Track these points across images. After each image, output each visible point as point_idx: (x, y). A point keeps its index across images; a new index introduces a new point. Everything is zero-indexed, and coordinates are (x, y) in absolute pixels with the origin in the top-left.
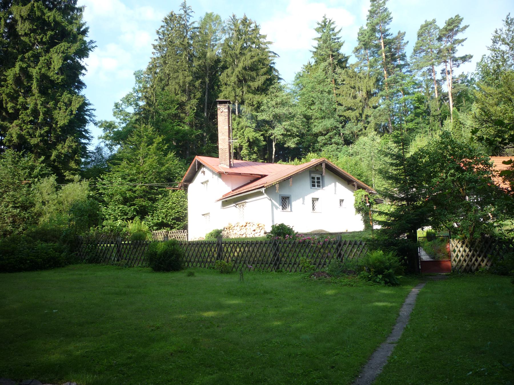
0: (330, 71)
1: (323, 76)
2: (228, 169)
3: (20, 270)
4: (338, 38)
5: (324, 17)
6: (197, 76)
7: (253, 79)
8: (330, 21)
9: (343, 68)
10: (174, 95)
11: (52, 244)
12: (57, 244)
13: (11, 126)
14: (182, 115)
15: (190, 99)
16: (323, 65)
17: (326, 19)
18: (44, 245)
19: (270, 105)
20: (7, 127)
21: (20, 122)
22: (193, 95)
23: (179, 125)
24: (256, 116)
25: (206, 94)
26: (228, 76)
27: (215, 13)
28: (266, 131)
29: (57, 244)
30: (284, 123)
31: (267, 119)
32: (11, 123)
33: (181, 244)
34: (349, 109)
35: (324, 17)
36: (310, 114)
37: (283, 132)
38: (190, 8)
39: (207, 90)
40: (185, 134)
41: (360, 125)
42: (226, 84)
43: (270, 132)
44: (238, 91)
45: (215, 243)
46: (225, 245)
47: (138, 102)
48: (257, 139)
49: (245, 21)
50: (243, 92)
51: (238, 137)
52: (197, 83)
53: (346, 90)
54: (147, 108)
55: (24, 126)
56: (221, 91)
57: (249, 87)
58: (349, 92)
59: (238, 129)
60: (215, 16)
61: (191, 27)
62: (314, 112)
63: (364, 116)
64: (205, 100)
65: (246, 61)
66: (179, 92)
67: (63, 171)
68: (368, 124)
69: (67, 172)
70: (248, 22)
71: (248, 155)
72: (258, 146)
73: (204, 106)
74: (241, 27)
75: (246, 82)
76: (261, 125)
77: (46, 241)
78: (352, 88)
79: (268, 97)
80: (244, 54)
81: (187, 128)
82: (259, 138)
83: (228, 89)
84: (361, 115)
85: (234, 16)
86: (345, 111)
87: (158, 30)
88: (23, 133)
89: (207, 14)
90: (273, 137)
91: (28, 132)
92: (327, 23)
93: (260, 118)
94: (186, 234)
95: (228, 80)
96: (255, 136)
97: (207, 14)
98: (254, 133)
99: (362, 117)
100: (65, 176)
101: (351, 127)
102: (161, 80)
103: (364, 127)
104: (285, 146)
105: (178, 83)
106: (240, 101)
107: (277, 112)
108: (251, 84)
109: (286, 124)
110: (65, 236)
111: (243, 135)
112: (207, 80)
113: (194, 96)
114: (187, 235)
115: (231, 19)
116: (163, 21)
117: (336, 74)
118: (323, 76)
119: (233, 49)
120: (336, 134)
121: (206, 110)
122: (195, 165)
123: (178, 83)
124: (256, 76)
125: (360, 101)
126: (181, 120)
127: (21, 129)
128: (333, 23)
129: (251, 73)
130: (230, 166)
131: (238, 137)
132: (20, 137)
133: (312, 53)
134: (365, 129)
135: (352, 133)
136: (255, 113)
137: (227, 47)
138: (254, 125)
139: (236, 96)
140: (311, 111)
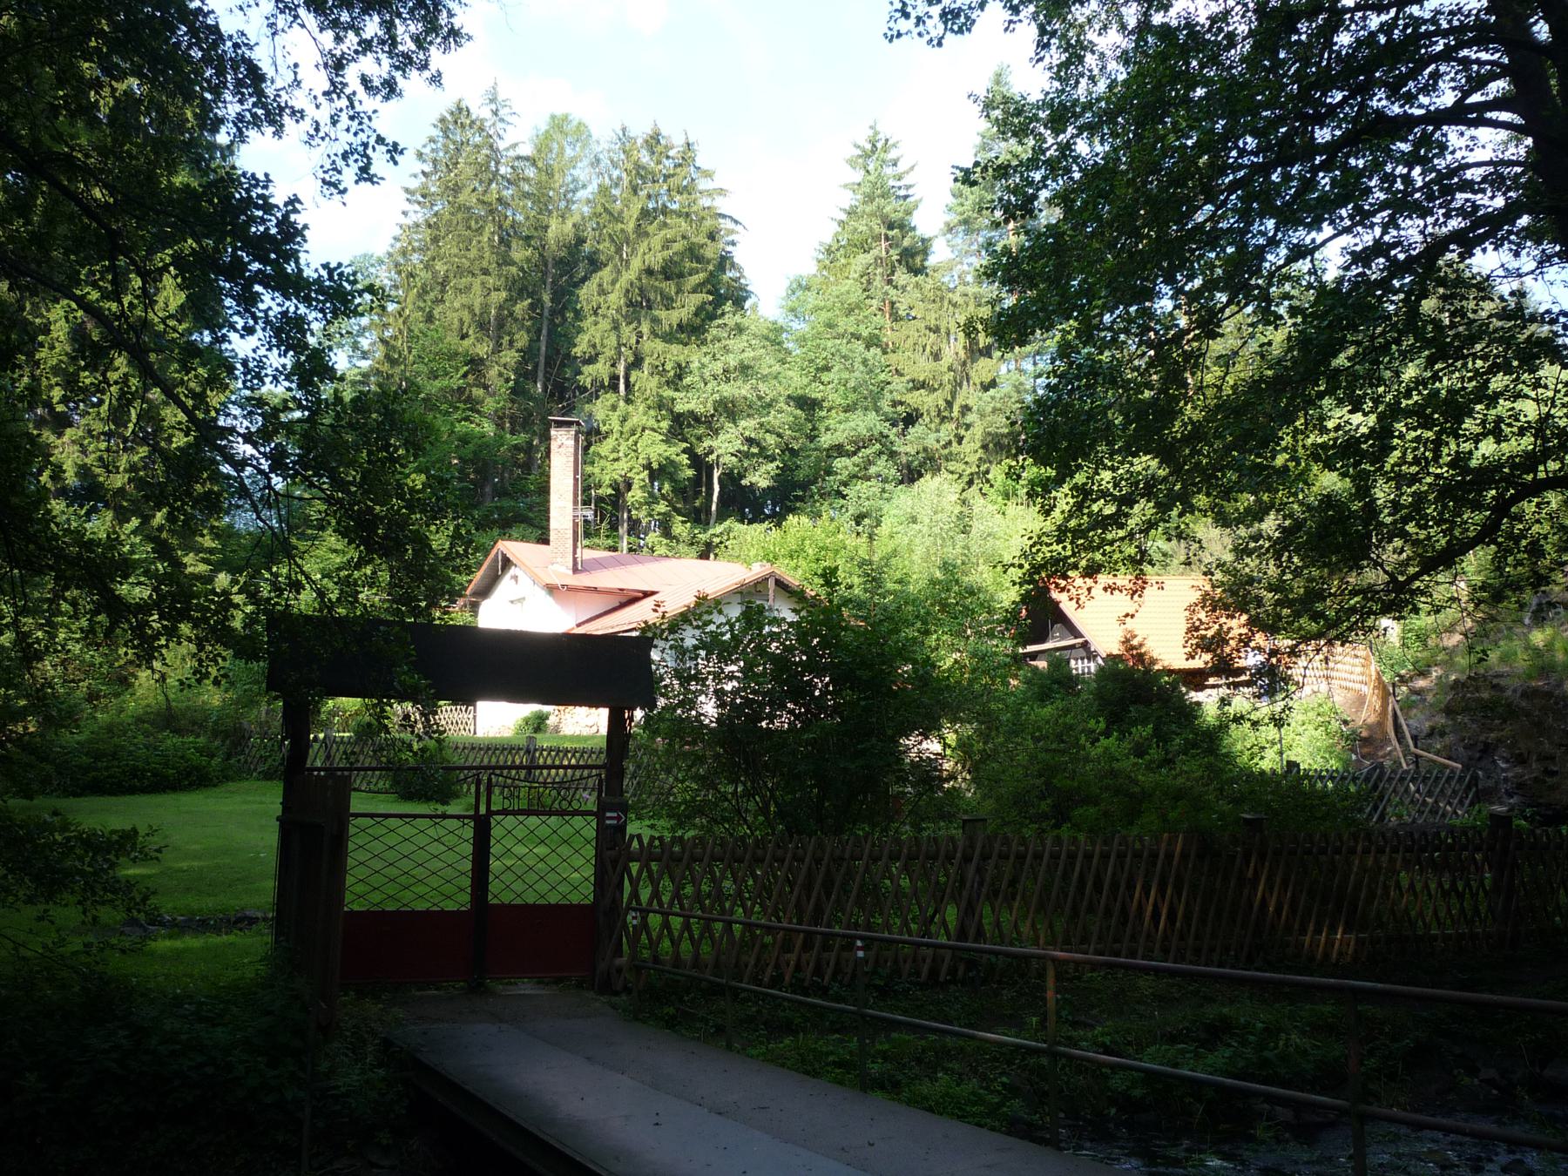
0: (878, 282)
1: (856, 295)
2: (567, 575)
3: (132, 791)
4: (908, 187)
5: (871, 127)
6: (519, 288)
7: (668, 303)
8: (887, 140)
9: (917, 271)
10: (457, 340)
11: (191, 739)
12: (202, 740)
13: (59, 441)
14: (478, 392)
15: (498, 348)
16: (863, 259)
17: (876, 133)
18: (177, 740)
19: (707, 374)
20: (49, 445)
21: (80, 433)
22: (508, 338)
23: (466, 419)
24: (673, 400)
25: (544, 332)
26: (602, 292)
27: (576, 116)
28: (699, 439)
29: (202, 740)
30: (743, 423)
31: (700, 409)
32: (60, 435)
33: (457, 748)
34: (918, 385)
35: (871, 127)
36: (819, 396)
37: (738, 445)
38: (508, 103)
39: (545, 323)
40: (483, 445)
41: (948, 430)
42: (595, 313)
43: (707, 443)
44: (627, 331)
45: (520, 749)
46: (541, 754)
47: (359, 339)
48: (672, 462)
49: (654, 141)
50: (640, 335)
51: (621, 454)
52: (521, 307)
53: (916, 334)
54: (386, 368)
55: (90, 443)
56: (580, 330)
57: (656, 321)
58: (922, 341)
59: (622, 433)
60: (575, 123)
61: (512, 153)
62: (829, 392)
63: (956, 408)
64: (539, 350)
65: (651, 253)
66: (471, 332)
67: (179, 553)
68: (967, 430)
69: (191, 555)
70: (663, 142)
71: (647, 503)
72: (672, 480)
73: (536, 366)
74: (645, 158)
75: (650, 308)
76: (681, 425)
77: (178, 731)
78: (930, 329)
79: (704, 349)
80: (647, 234)
81: (488, 428)
82: (678, 459)
83: (599, 326)
84: (950, 404)
85: (624, 130)
86: (910, 390)
87: (420, 148)
88: (88, 461)
89: (553, 117)
90: (713, 457)
91: (101, 459)
92: (879, 145)
93: (680, 408)
94: (471, 716)
95: (601, 300)
96: (667, 454)
97: (553, 117)
98: (664, 447)
99: (951, 412)
100: (185, 566)
101: (922, 437)
102: (424, 292)
103: (956, 435)
104: (743, 482)
105: (470, 308)
106: (631, 359)
107: (725, 394)
108: (662, 314)
109: (748, 425)
110: (215, 723)
111: (635, 451)
112: (546, 298)
113: (511, 343)
114: (475, 717)
115: (615, 137)
116: (435, 126)
117: (896, 287)
118: (856, 295)
119: (618, 218)
120: (881, 453)
121: (541, 375)
122: (495, 560)
123: (470, 308)
124: (677, 293)
125: (950, 369)
126: (473, 405)
127: (84, 452)
128: (894, 145)
129: (663, 285)
130: (575, 570)
131: (621, 454)
132: (84, 471)
133: (836, 224)
134: (960, 443)
135: (925, 450)
136: (668, 393)
137: (607, 213)
138: (665, 425)
139: (619, 345)
140: (822, 387)
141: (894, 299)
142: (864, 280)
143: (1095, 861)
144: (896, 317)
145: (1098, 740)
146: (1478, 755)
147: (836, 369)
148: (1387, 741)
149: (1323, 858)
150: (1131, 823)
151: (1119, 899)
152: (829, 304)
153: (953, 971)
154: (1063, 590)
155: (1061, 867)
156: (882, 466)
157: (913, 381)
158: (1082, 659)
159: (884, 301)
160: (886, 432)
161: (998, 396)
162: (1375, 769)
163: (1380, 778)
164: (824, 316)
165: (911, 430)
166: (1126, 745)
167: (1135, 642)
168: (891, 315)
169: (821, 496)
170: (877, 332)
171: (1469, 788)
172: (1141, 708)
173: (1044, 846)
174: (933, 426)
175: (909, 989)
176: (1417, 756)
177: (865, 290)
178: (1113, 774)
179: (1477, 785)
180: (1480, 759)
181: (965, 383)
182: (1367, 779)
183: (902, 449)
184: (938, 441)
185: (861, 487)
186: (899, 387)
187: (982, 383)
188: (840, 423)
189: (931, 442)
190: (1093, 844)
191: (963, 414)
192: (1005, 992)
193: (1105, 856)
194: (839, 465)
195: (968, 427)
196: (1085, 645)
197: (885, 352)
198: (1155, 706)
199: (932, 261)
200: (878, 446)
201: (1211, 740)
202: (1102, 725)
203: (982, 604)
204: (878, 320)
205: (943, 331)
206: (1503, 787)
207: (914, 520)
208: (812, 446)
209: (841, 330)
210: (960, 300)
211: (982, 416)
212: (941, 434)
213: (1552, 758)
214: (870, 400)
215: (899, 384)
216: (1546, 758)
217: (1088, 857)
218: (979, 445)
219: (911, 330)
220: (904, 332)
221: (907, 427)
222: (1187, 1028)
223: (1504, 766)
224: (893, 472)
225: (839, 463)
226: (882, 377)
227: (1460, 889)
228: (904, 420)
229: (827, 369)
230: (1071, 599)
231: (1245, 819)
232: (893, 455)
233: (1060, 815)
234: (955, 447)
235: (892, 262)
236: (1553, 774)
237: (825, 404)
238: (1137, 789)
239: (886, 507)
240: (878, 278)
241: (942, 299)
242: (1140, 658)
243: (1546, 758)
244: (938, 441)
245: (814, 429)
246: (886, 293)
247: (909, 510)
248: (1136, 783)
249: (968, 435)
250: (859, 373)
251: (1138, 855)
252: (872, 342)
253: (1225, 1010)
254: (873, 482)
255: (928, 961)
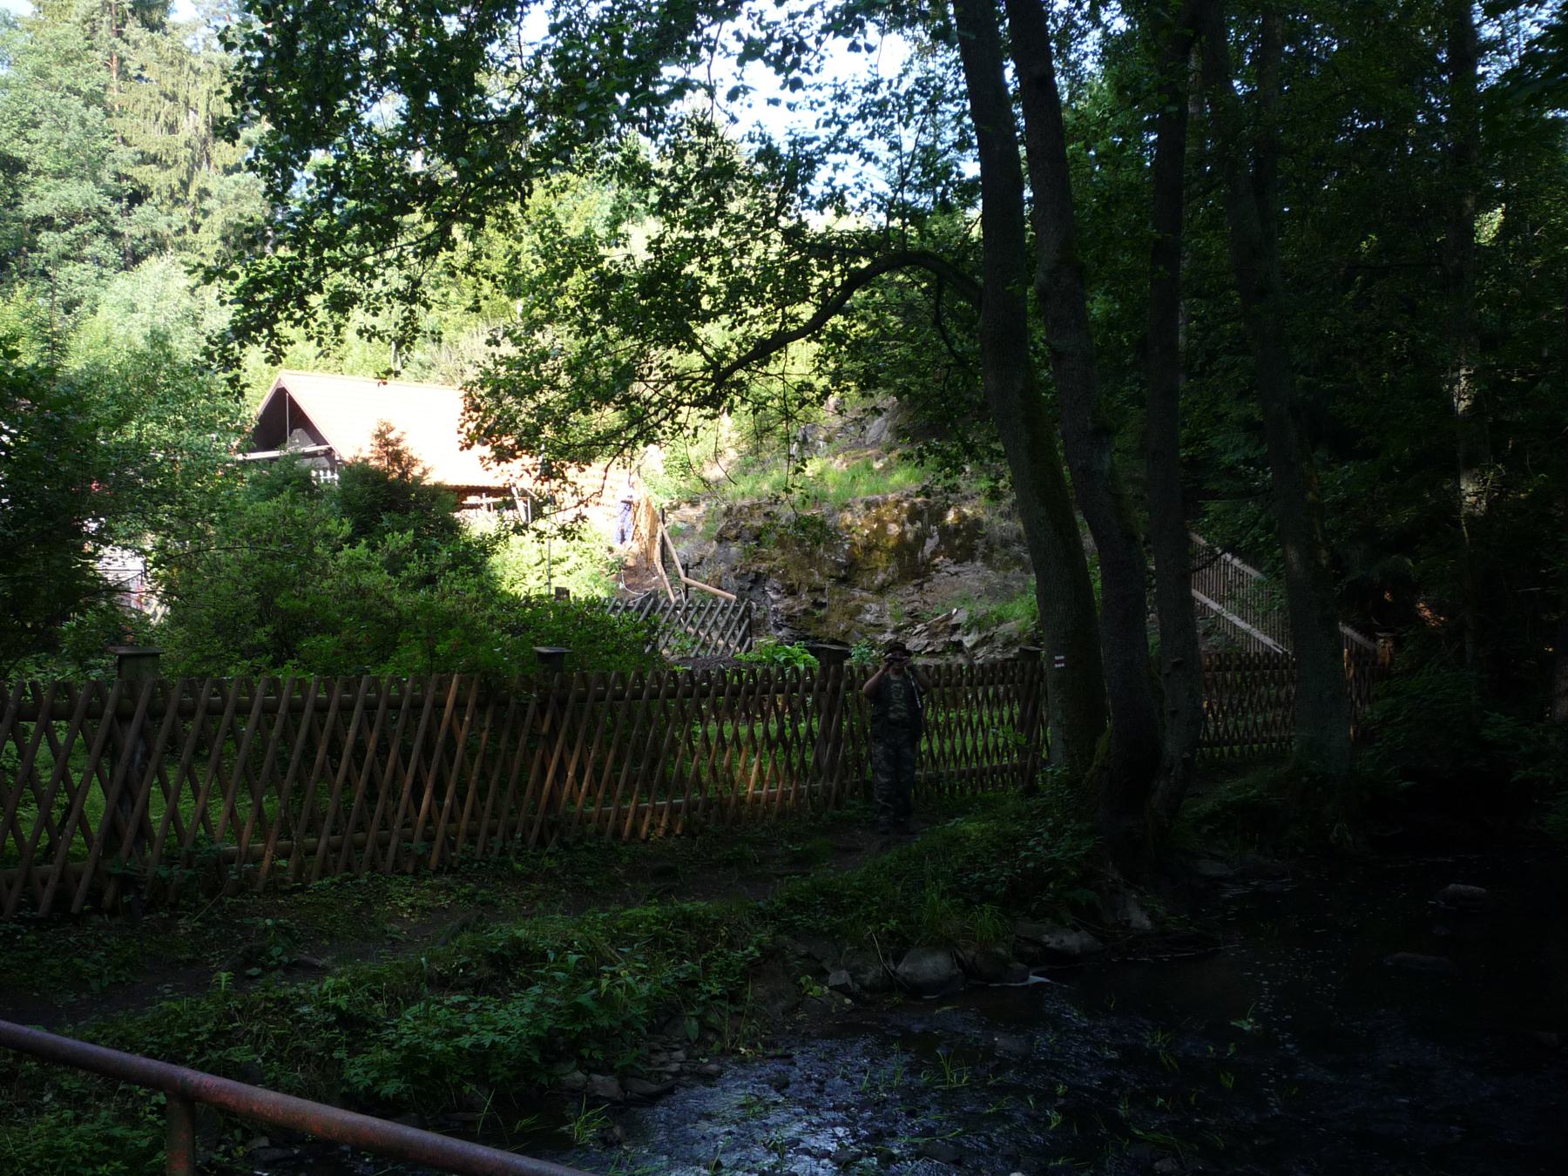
0: (104, 31)
1: (77, 41)
34: (147, 159)
36: (23, 155)
41: (181, 216)
53: (148, 99)
58: (155, 108)
63: (193, 191)
78: (166, 96)
84: (185, 185)
99: (187, 194)
103: (192, 222)
117: (126, 41)
118: (77, 41)
120: (98, 232)
125: (188, 144)
134: (196, 230)
135: (154, 234)
140: (26, 145)
141: (124, 54)
142: (87, 27)
143: (331, 715)
144: (123, 74)
145: (341, 549)
146: (748, 585)
147: (46, 124)
148: (653, 572)
149: (672, 704)
150: (385, 659)
151: (366, 768)
152: (42, 49)
153: (95, 895)
154: (298, 322)
155: (278, 723)
156: (98, 246)
157: (142, 153)
158: (325, 470)
159: (111, 54)
160: (105, 207)
161: (242, 181)
162: (648, 598)
163: (653, 608)
164: (34, 61)
165: (136, 208)
166: (379, 558)
167: (391, 436)
168: (119, 74)
169: (23, 275)
170: (100, 89)
171: (742, 620)
172: (396, 516)
173: (252, 695)
174: (164, 208)
175: (16, 931)
176: (687, 586)
177: (87, 39)
178: (361, 592)
179: (749, 617)
180: (750, 589)
181: (204, 163)
182: (640, 609)
183: (126, 231)
184: (170, 226)
185: (72, 269)
186: (125, 157)
187: (225, 166)
188: (48, 189)
189: (161, 225)
190: (329, 690)
191: (201, 199)
192: (182, 921)
193: (346, 709)
194: (45, 240)
195: (206, 213)
196: (329, 453)
197: (108, 115)
198: (412, 514)
199: (173, 19)
200: (95, 223)
201: (474, 557)
202: (347, 529)
203: (200, 387)
204: (103, 75)
205: (181, 99)
206: (771, 620)
207: (133, 308)
208: (12, 214)
209: (54, 81)
210: (204, 68)
211: (223, 202)
212: (174, 219)
213: (822, 590)
214: (90, 168)
215: (124, 154)
216: (816, 590)
217: (321, 709)
218: (218, 235)
219: (141, 92)
220: (134, 95)
221: (130, 206)
222: (465, 966)
223: (774, 597)
224: (113, 256)
225: (45, 238)
226: (104, 143)
227: (788, 736)
228: (129, 197)
229: (36, 125)
230: (310, 338)
231: (540, 654)
232: (114, 235)
233: (283, 648)
234: (189, 235)
235: (124, 12)
236: (822, 606)
237: (29, 167)
238: (391, 614)
239: (103, 295)
240: (104, 26)
241: (182, 62)
242: (396, 457)
243: (816, 590)
244: (170, 226)
245: (16, 195)
246: (114, 46)
247: (128, 296)
248: (390, 604)
249: (206, 223)
250: (75, 132)
251: (394, 705)
252: (92, 99)
253: (520, 933)
254: (88, 265)
255: (52, 882)
